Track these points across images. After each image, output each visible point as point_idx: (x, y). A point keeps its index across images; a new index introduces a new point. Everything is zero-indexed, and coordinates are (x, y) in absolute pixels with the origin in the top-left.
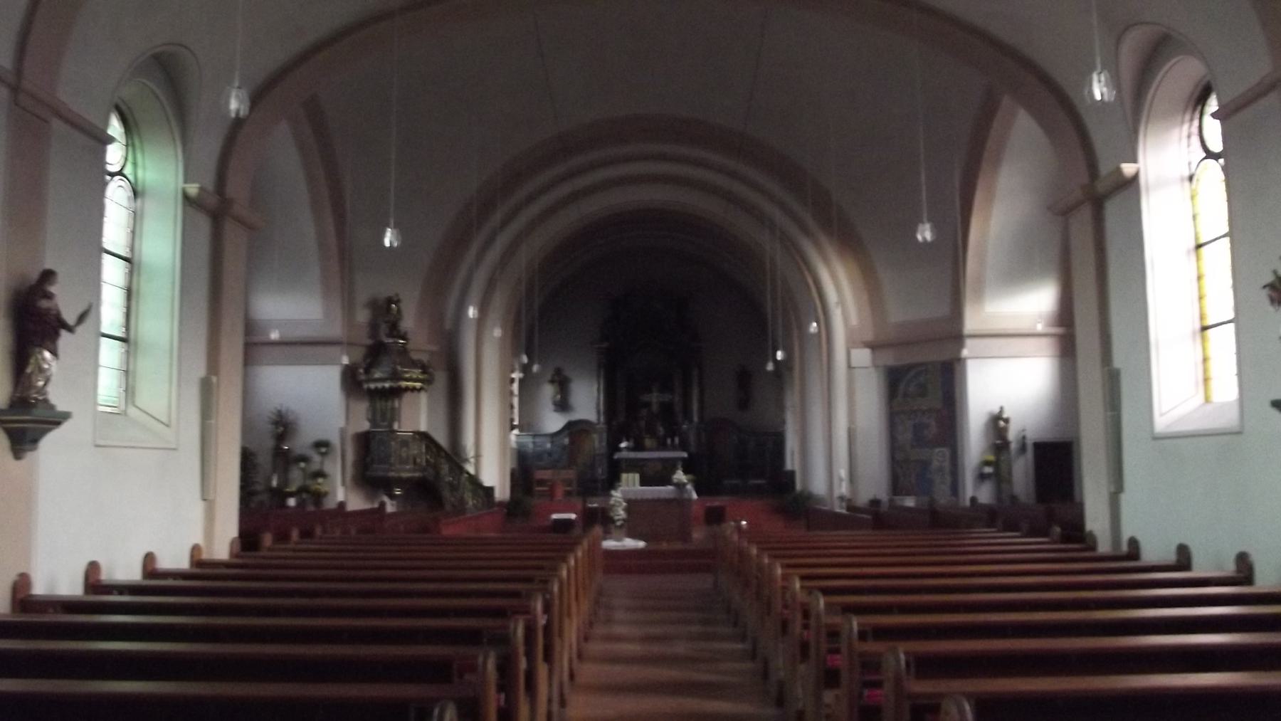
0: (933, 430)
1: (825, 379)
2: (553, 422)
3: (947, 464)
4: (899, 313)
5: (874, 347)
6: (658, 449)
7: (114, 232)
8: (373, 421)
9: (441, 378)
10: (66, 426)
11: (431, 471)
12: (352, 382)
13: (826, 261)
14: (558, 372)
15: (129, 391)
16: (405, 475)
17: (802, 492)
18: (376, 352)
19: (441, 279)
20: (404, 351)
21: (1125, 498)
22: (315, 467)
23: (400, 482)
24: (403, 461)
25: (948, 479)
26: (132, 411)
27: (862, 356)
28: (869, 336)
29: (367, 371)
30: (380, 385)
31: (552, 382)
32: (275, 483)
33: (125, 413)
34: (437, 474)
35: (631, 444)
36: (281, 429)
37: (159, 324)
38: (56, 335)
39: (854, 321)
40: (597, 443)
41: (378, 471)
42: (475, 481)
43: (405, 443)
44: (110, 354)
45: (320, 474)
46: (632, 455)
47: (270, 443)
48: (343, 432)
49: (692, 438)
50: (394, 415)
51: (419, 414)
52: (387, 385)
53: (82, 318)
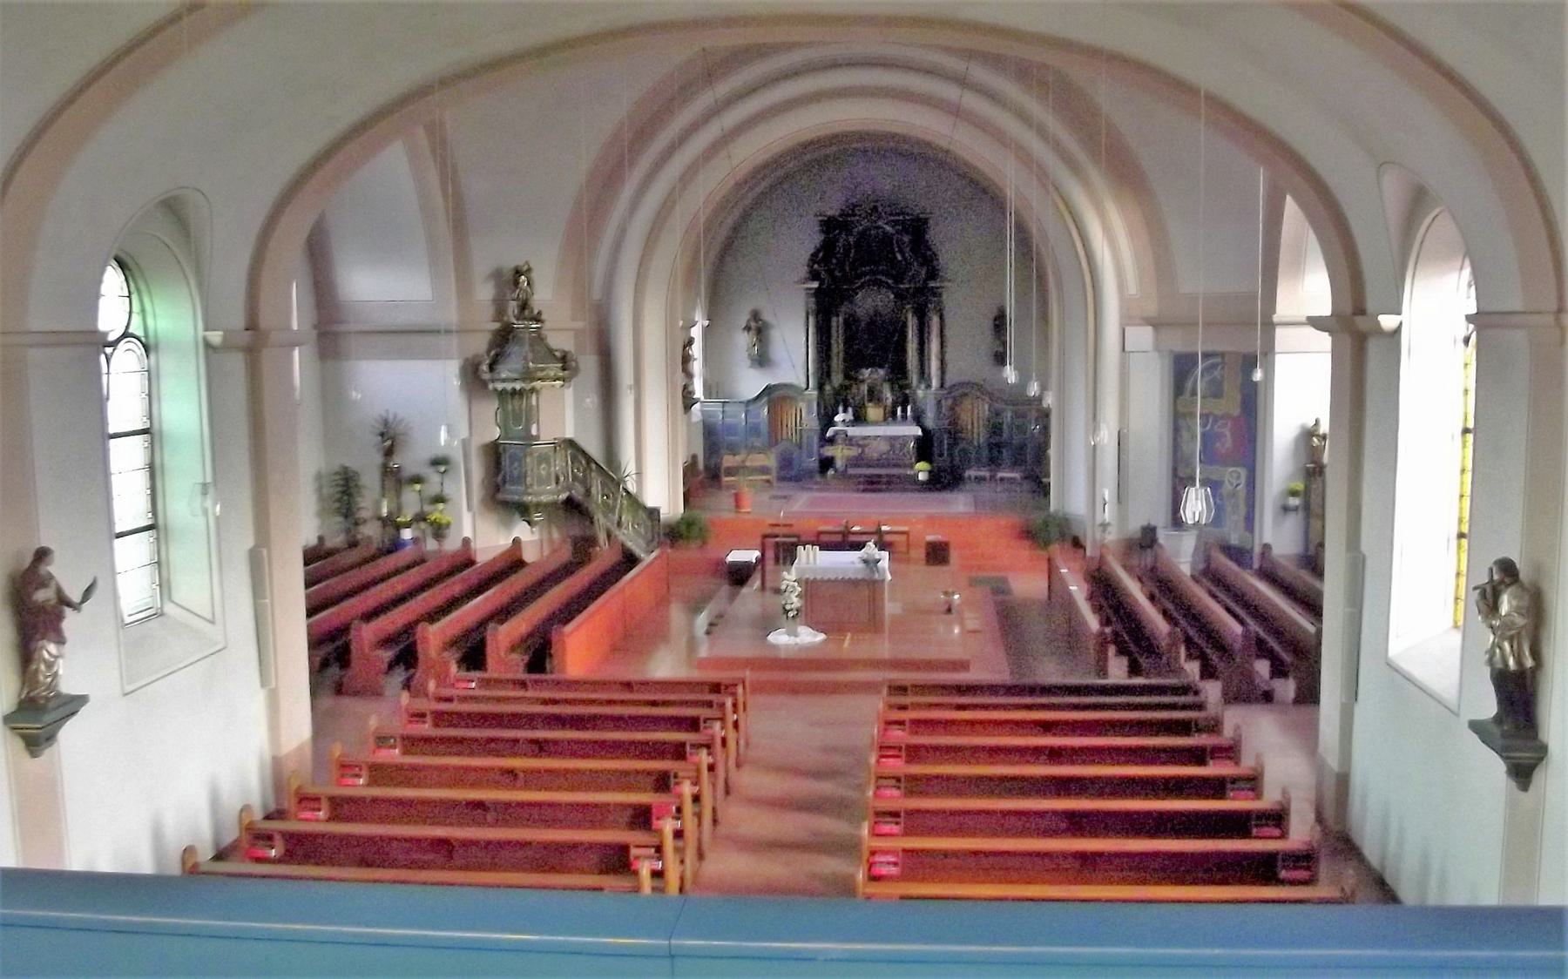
0: (1227, 443)
1: (1091, 364)
2: (751, 383)
5: (1157, 324)
7: (125, 408)
8: (504, 427)
9: (589, 364)
12: (474, 378)
14: (756, 316)
15: (164, 586)
16: (544, 499)
17: (1056, 511)
18: (504, 338)
20: (539, 338)
22: (432, 488)
24: (542, 481)
25: (1243, 510)
26: (169, 608)
27: (1142, 337)
28: (1151, 308)
29: (492, 368)
30: (509, 386)
33: (160, 614)
34: (588, 492)
36: (389, 443)
38: (60, 617)
39: (1133, 289)
41: (512, 493)
42: (634, 502)
43: (543, 459)
44: (132, 555)
47: (378, 459)
48: (465, 444)
50: (529, 416)
51: (563, 414)
53: (88, 593)
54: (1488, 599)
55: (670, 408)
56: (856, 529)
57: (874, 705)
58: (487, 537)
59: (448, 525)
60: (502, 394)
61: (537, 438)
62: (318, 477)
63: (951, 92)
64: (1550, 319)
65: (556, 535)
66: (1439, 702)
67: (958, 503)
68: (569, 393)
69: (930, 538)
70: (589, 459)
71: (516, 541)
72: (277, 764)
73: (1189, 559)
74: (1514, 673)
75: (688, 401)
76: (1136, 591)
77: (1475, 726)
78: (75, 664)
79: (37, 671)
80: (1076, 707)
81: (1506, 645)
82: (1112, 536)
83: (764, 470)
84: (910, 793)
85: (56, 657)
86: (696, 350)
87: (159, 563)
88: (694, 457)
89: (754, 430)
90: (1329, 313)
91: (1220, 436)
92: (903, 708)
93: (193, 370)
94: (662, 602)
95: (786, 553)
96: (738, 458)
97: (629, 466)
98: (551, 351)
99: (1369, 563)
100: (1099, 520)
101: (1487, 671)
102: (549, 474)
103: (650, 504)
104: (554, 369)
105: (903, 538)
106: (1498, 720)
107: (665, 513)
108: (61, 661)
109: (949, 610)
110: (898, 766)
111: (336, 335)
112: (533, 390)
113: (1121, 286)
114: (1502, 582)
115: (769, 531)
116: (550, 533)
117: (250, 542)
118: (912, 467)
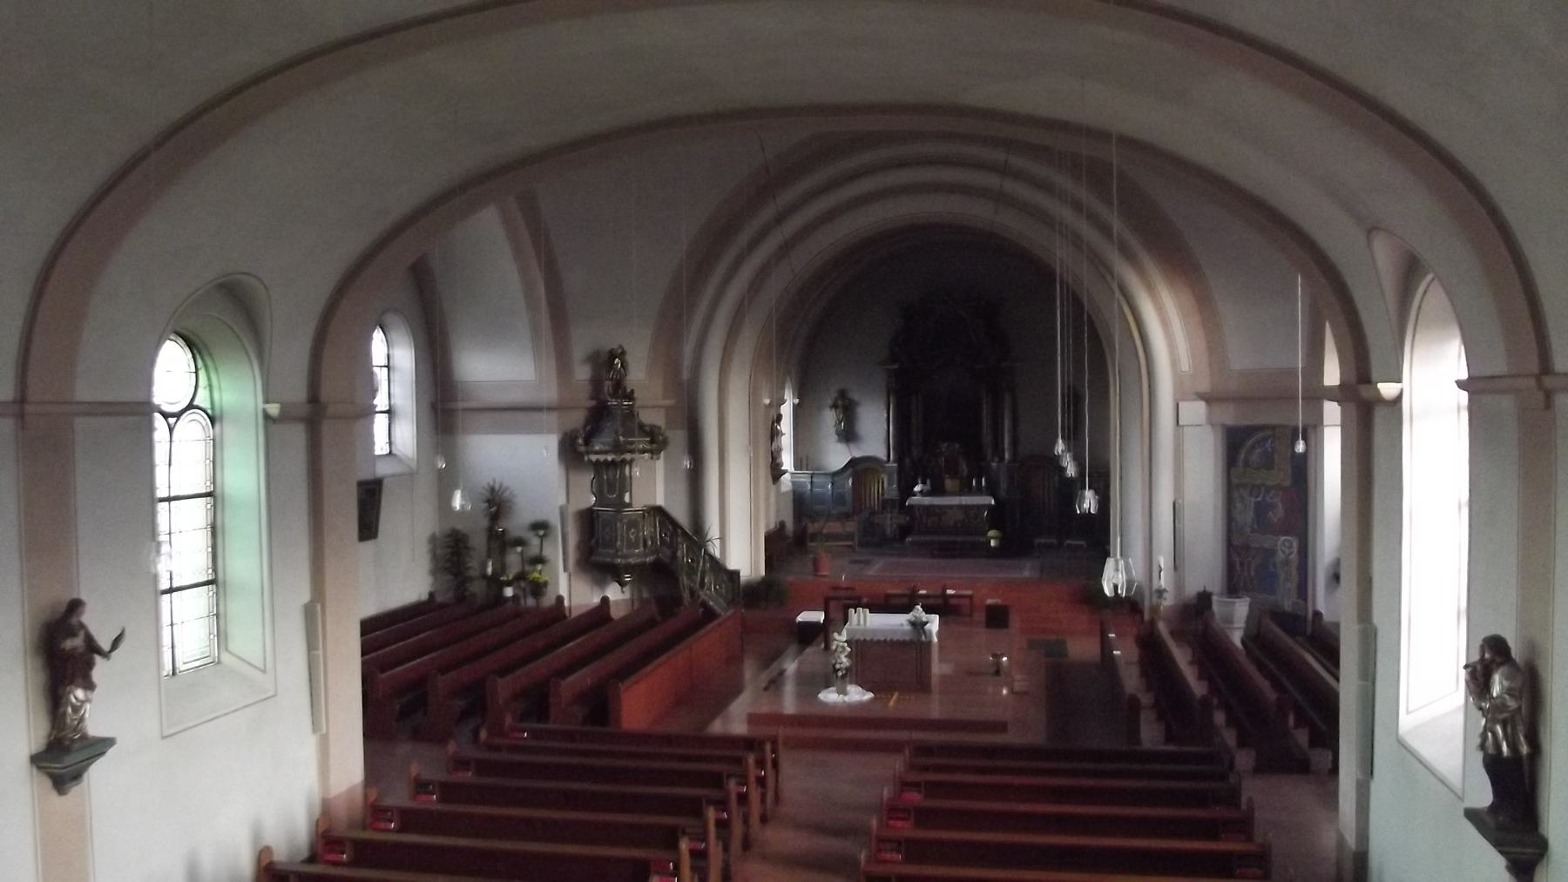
0: (1278, 514)
2: (837, 456)
3: (1294, 557)
4: (1242, 358)
5: (1209, 399)
6: (961, 493)
8: (599, 494)
9: (678, 438)
10: (111, 752)
11: (668, 552)
12: (572, 452)
13: (1150, 288)
14: (843, 394)
15: (221, 635)
18: (598, 416)
19: (675, 317)
20: (631, 414)
21: (1376, 786)
22: (534, 550)
23: (629, 568)
26: (225, 657)
27: (1195, 411)
28: (1204, 385)
29: (587, 442)
30: (602, 458)
31: (835, 406)
32: (490, 570)
34: (674, 556)
35: (928, 487)
37: (246, 563)
38: (90, 665)
39: (1185, 365)
40: (886, 485)
41: (604, 555)
42: (717, 566)
43: (632, 524)
45: (539, 560)
46: (927, 501)
47: (485, 523)
48: (563, 512)
49: (1003, 486)
50: (624, 485)
51: (653, 485)
52: (610, 458)
53: (116, 643)
54: (1478, 678)
55: (754, 482)
56: (923, 592)
57: (895, 764)
58: (572, 591)
59: (545, 584)
60: (598, 467)
61: (630, 505)
62: (433, 539)
63: (990, 180)
64: (1532, 382)
65: (645, 595)
66: (1442, 781)
67: (1027, 570)
68: (660, 464)
69: (989, 601)
70: (675, 524)
71: (605, 600)
72: (327, 807)
73: (1243, 625)
74: (1507, 760)
75: (776, 472)
76: (1181, 657)
77: (1472, 815)
78: (98, 711)
79: (65, 713)
80: (1096, 774)
81: (1499, 729)
82: (1168, 601)
83: (849, 537)
84: (908, 859)
85: (83, 702)
86: (786, 426)
87: (218, 616)
88: (782, 525)
89: (839, 499)
90: (1337, 383)
91: (1272, 506)
92: (926, 769)
93: (253, 440)
94: (735, 660)
95: (837, 619)
96: (816, 525)
97: (713, 531)
98: (641, 426)
99: (1380, 634)
100: (1155, 586)
101: (1480, 756)
102: (637, 538)
103: (732, 564)
104: (642, 442)
105: (967, 601)
106: (1493, 809)
107: (745, 575)
108: (88, 706)
109: (997, 672)
110: (906, 829)
111: (453, 411)
112: (624, 462)
113: (1174, 362)
114: (1492, 661)
115: (832, 594)
116: (640, 591)
117: (306, 597)
118: (985, 534)
